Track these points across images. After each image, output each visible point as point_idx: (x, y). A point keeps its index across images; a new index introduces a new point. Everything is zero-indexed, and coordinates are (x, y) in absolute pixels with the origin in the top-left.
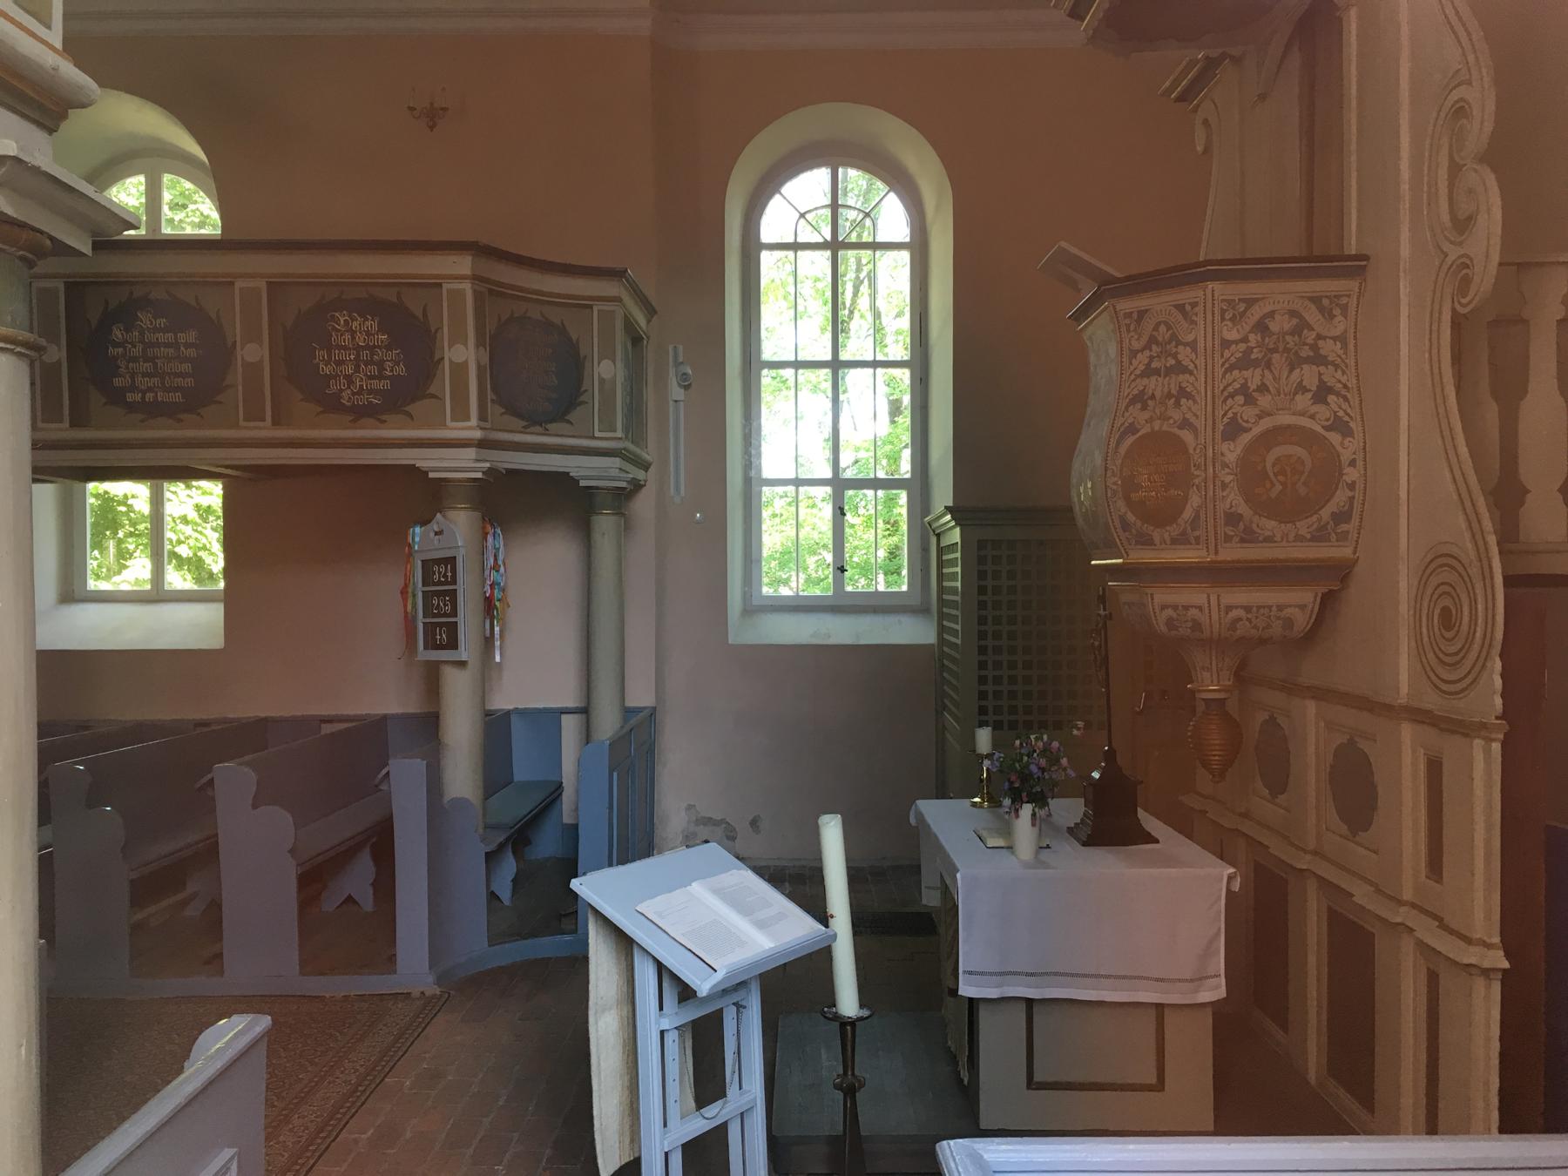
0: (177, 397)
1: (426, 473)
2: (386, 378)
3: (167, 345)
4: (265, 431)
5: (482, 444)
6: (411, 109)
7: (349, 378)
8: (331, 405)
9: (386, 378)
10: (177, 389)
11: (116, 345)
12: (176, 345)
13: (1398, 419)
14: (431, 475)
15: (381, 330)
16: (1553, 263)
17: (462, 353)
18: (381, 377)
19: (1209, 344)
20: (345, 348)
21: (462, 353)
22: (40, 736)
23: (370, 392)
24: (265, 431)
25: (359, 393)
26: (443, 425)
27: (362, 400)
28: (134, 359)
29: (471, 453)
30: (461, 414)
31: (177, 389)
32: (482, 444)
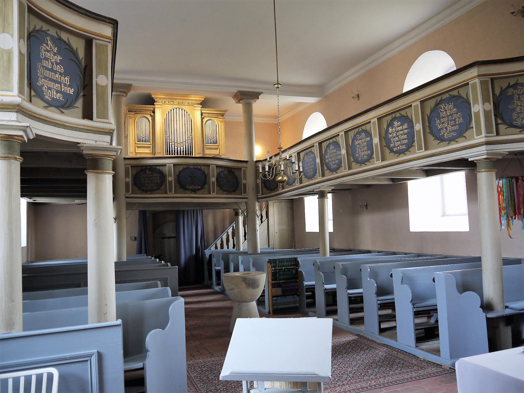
0: (404, 147)
1: (468, 159)
2: (457, 125)
3: (401, 130)
4: (423, 153)
5: (487, 143)
6: (512, 13)
7: (446, 128)
8: (441, 140)
9: (457, 125)
10: (403, 145)
11: (391, 134)
12: (402, 130)
13: (472, 95)
14: (470, 160)
15: (454, 107)
16: (444, 10)
17: (478, 108)
18: (455, 125)
19: (181, 131)
20: (444, 117)
21: (478, 108)
22: (481, 270)
23: (453, 131)
24: (423, 153)
25: (449, 133)
26: (473, 138)
27: (450, 135)
28: (394, 137)
29: (484, 148)
30: (479, 133)
31: (403, 145)
32: (487, 143)
